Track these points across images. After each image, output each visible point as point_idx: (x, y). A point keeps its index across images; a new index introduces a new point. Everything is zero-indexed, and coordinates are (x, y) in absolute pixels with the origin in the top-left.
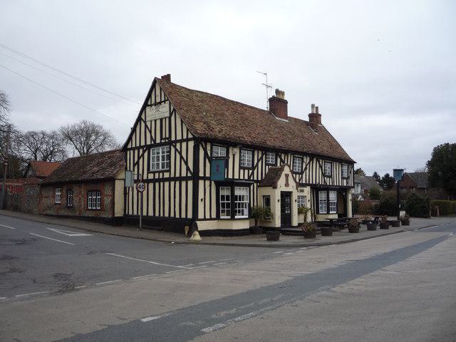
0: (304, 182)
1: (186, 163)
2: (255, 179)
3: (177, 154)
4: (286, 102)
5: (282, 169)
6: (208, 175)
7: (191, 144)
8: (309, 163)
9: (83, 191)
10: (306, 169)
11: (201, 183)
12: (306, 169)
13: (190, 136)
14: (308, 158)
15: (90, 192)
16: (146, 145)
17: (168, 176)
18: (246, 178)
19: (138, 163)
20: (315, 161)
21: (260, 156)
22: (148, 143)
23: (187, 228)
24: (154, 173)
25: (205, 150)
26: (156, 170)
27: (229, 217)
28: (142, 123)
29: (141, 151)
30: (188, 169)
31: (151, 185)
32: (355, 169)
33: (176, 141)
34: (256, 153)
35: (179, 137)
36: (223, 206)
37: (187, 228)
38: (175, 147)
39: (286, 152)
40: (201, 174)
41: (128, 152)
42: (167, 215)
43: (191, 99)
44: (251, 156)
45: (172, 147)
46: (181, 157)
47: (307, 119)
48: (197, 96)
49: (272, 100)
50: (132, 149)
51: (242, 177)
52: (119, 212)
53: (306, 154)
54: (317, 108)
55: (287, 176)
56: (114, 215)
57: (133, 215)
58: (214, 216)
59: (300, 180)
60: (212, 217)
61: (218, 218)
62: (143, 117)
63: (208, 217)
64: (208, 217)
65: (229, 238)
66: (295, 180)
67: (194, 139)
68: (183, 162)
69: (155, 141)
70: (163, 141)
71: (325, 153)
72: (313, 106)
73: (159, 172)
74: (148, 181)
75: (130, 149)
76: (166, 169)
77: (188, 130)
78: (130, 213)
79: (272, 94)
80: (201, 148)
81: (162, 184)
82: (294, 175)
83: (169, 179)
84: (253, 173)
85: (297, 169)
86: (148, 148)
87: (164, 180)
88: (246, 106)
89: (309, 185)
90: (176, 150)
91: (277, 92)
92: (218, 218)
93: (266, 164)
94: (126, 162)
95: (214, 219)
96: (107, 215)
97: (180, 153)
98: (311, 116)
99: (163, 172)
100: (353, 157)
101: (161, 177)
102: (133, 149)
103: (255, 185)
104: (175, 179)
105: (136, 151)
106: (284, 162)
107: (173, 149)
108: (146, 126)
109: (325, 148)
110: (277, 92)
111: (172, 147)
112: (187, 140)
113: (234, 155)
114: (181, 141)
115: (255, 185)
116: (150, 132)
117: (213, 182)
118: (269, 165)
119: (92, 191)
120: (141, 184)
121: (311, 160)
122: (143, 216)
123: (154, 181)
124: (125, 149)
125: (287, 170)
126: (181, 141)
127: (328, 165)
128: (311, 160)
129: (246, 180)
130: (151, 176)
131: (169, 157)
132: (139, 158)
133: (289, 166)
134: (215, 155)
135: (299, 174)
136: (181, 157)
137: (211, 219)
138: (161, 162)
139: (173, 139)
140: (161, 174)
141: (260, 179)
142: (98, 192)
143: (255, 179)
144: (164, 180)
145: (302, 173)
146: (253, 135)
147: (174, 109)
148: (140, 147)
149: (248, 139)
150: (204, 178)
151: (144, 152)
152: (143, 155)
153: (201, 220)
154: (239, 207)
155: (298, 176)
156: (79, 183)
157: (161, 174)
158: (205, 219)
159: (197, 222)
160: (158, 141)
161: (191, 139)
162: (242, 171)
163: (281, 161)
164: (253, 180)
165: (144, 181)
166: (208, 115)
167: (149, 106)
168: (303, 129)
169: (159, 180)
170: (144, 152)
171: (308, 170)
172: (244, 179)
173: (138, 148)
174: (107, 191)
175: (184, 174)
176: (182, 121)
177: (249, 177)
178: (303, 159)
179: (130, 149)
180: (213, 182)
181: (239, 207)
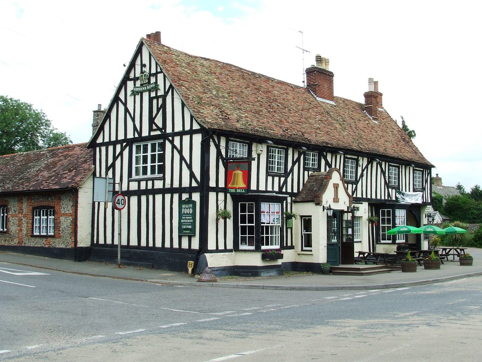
0: (359, 196)
1: (190, 167)
2: (289, 190)
3: (176, 153)
4: (330, 75)
5: (328, 176)
6: (222, 185)
7: (198, 139)
8: (367, 167)
9: (26, 207)
10: (362, 176)
11: (212, 196)
12: (362, 176)
13: (196, 127)
14: (365, 160)
15: (36, 210)
16: (126, 140)
17: (161, 186)
18: (276, 189)
19: (113, 165)
20: (375, 164)
21: (296, 156)
22: (130, 136)
23: (190, 265)
24: (139, 181)
25: (218, 147)
26: (141, 176)
27: (253, 248)
28: (121, 107)
29: (118, 147)
30: (192, 175)
31: (134, 200)
32: (434, 175)
33: (174, 134)
34: (290, 151)
35: (178, 128)
36: (243, 232)
37: (190, 265)
38: (172, 142)
39: (334, 151)
40: (212, 184)
41: (98, 149)
42: (159, 244)
43: (195, 71)
44: (283, 155)
45: (167, 142)
46: (182, 158)
47: (362, 101)
48: (202, 65)
49: (310, 72)
50: (103, 144)
51: (270, 189)
52: (84, 241)
53: (360, 153)
54: (376, 83)
55: (336, 186)
56: (76, 242)
57: (105, 245)
58: (230, 246)
59: (353, 193)
60: (220, 248)
61: (236, 248)
62: (122, 96)
63: (221, 247)
64: (221, 247)
65: (252, 278)
66: (346, 189)
67: (202, 130)
68: (184, 165)
69: (140, 133)
70: (153, 133)
71: (391, 152)
72: (371, 80)
73: (147, 180)
74: (129, 193)
75: (100, 145)
76: (157, 175)
77: (192, 117)
78: (101, 241)
79: (312, 62)
80: (212, 144)
81: (151, 197)
82: (390, 190)
83: (163, 191)
84: (285, 182)
85: (350, 176)
86: (129, 142)
87: (154, 192)
88: (273, 80)
89: (366, 200)
90: (174, 147)
91: (319, 59)
92: (236, 248)
93: (305, 169)
94: (95, 164)
95: (231, 251)
96: (59, 244)
97: (180, 152)
98: (368, 96)
99: (153, 180)
100: (429, 157)
101: (150, 187)
102: (107, 145)
103: (289, 199)
104: (172, 191)
105: (111, 148)
106: (330, 166)
107: (168, 146)
108: (127, 110)
109: (389, 145)
110: (319, 59)
111: (167, 142)
112: (192, 132)
113: (259, 155)
114: (181, 134)
115: (289, 199)
116: (133, 119)
117: (228, 195)
118: (308, 170)
119: (40, 208)
120: (120, 197)
121: (370, 162)
122: (347, 235)
123: (139, 193)
124: (93, 145)
125: (336, 178)
126: (181, 134)
127: (394, 171)
128: (370, 162)
129: (276, 193)
130: (134, 186)
131: (162, 158)
132: (115, 159)
133: (339, 171)
134: (230, 154)
135: (352, 183)
136: (182, 158)
137: (225, 250)
138: (149, 165)
139: (169, 130)
140: (150, 183)
141: (295, 191)
142: (50, 210)
143: (289, 190)
144: (154, 192)
145: (356, 182)
146: (286, 125)
147: (171, 86)
148: (117, 142)
149: (277, 132)
150: (217, 190)
151: (123, 149)
152: (121, 154)
153: (211, 252)
154: (267, 233)
155: (350, 186)
156: (19, 195)
157: (150, 183)
158: (217, 251)
159: (207, 255)
160: (145, 133)
161: (197, 132)
162: (270, 178)
163: (327, 163)
164: (286, 193)
165: (124, 194)
166: (220, 95)
167: (131, 80)
168: (357, 116)
169: (147, 192)
170: (123, 149)
171: (364, 178)
172: (273, 192)
173: (114, 144)
174: (65, 207)
175: (186, 183)
176: (183, 105)
177: (280, 188)
178: (357, 161)
179: (100, 145)
180: (228, 195)
181: (267, 233)
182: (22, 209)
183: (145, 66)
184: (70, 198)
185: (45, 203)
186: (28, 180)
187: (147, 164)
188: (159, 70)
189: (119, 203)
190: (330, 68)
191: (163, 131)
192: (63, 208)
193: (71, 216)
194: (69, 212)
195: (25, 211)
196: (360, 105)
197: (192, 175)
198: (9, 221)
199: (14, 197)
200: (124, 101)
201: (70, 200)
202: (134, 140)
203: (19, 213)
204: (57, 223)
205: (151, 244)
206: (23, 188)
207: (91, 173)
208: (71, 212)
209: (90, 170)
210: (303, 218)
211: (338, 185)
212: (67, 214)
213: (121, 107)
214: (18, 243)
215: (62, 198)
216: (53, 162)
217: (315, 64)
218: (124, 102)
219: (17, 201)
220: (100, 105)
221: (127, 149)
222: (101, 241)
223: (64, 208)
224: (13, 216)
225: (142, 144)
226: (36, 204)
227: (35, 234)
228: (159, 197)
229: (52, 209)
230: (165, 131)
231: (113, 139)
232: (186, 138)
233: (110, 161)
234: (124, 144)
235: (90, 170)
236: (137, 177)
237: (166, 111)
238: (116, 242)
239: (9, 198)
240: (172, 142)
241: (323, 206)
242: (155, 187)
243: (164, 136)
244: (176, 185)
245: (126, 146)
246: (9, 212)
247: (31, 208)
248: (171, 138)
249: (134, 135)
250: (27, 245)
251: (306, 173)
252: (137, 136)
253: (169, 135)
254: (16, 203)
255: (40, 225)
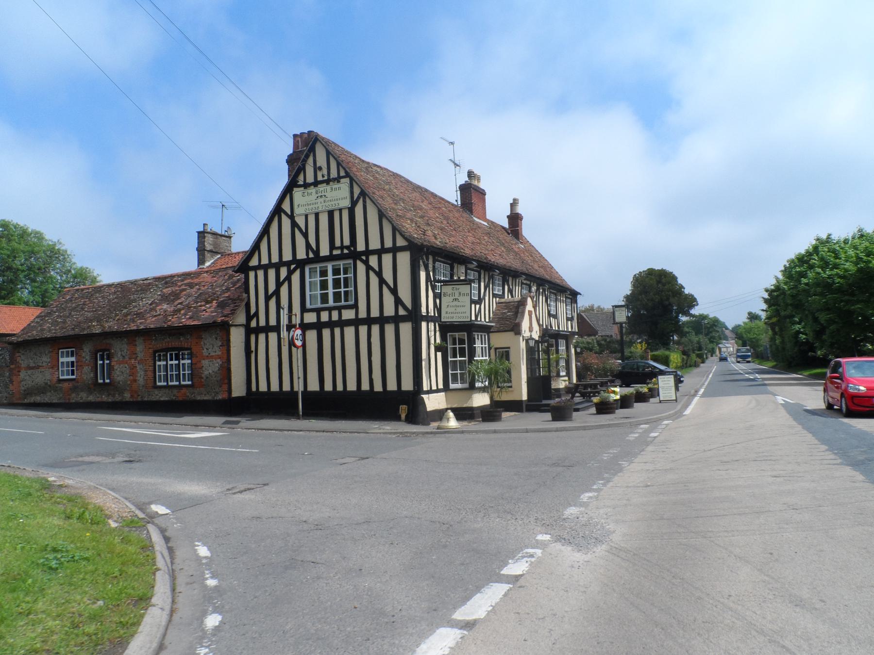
7: (404, 259)
9: (141, 348)
15: (158, 354)
16: (295, 260)
22: (301, 254)
23: (403, 410)
24: (318, 311)
35: (375, 245)
37: (403, 410)
38: (366, 263)
46: (382, 282)
52: (238, 390)
62: (286, 206)
63: (434, 388)
69: (317, 252)
70: (336, 252)
75: (255, 269)
81: (337, 331)
82: (551, 318)
83: (356, 323)
87: (342, 324)
91: (470, 174)
102: (265, 268)
105: (272, 273)
107: (361, 268)
108: (294, 225)
112: (395, 250)
116: (305, 235)
126: (380, 252)
136: (382, 282)
138: (331, 291)
139: (361, 247)
144: (342, 324)
148: (281, 263)
151: (290, 273)
152: (288, 278)
156: (131, 336)
161: (402, 249)
169: (331, 325)
170: (290, 273)
173: (277, 266)
175: (389, 311)
179: (255, 269)
182: (136, 354)
183: (320, 168)
184: (216, 336)
185: (176, 344)
186: (140, 315)
187: (328, 290)
188: (342, 173)
189: (298, 339)
190: (482, 185)
191: (352, 249)
192: (205, 350)
193: (220, 358)
194: (217, 354)
195: (140, 356)
196: (504, 228)
197: (398, 302)
198: (114, 370)
199: (120, 337)
200: (289, 213)
201: (216, 339)
202: (308, 261)
203: (130, 359)
204: (195, 369)
205: (340, 388)
206: (137, 326)
207: (244, 303)
208: (220, 353)
209: (242, 300)
210: (497, 350)
211: (531, 311)
212: (212, 356)
213: (286, 222)
214: (130, 398)
215: (203, 336)
216: (173, 292)
217: (467, 179)
218: (290, 214)
219: (127, 344)
220: (205, 225)
221: (298, 273)
222: (263, 388)
223: (207, 349)
224: (119, 363)
225: (318, 266)
226: (160, 346)
227: (158, 384)
228: (350, 331)
229: (174, 351)
230: (355, 248)
231: (275, 259)
232: (387, 259)
233: (272, 287)
234: (293, 267)
235: (242, 300)
236: (313, 307)
237: (355, 225)
238: (299, 387)
239: (113, 340)
240: (366, 263)
241: (523, 336)
242: (343, 318)
243: (355, 255)
244: (375, 313)
245: (295, 269)
246: (113, 358)
247: (151, 351)
248: (364, 258)
249: (307, 254)
250: (146, 399)
251: (494, 299)
252: (311, 255)
253: (362, 253)
254: (126, 346)
255: (167, 372)
